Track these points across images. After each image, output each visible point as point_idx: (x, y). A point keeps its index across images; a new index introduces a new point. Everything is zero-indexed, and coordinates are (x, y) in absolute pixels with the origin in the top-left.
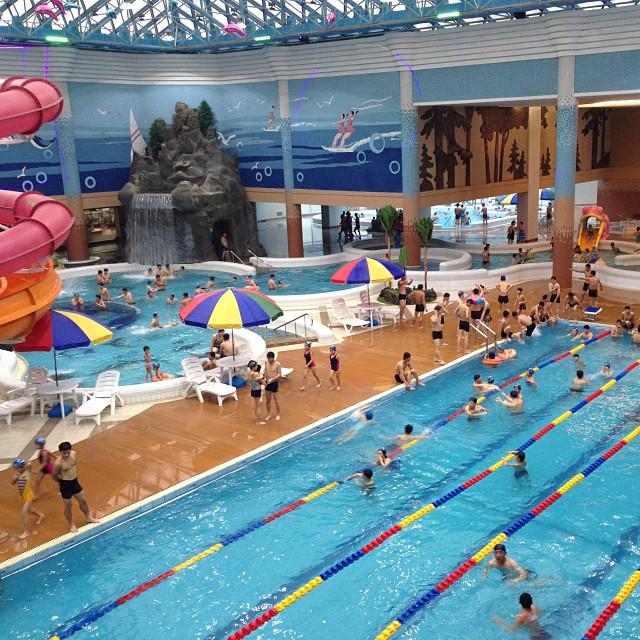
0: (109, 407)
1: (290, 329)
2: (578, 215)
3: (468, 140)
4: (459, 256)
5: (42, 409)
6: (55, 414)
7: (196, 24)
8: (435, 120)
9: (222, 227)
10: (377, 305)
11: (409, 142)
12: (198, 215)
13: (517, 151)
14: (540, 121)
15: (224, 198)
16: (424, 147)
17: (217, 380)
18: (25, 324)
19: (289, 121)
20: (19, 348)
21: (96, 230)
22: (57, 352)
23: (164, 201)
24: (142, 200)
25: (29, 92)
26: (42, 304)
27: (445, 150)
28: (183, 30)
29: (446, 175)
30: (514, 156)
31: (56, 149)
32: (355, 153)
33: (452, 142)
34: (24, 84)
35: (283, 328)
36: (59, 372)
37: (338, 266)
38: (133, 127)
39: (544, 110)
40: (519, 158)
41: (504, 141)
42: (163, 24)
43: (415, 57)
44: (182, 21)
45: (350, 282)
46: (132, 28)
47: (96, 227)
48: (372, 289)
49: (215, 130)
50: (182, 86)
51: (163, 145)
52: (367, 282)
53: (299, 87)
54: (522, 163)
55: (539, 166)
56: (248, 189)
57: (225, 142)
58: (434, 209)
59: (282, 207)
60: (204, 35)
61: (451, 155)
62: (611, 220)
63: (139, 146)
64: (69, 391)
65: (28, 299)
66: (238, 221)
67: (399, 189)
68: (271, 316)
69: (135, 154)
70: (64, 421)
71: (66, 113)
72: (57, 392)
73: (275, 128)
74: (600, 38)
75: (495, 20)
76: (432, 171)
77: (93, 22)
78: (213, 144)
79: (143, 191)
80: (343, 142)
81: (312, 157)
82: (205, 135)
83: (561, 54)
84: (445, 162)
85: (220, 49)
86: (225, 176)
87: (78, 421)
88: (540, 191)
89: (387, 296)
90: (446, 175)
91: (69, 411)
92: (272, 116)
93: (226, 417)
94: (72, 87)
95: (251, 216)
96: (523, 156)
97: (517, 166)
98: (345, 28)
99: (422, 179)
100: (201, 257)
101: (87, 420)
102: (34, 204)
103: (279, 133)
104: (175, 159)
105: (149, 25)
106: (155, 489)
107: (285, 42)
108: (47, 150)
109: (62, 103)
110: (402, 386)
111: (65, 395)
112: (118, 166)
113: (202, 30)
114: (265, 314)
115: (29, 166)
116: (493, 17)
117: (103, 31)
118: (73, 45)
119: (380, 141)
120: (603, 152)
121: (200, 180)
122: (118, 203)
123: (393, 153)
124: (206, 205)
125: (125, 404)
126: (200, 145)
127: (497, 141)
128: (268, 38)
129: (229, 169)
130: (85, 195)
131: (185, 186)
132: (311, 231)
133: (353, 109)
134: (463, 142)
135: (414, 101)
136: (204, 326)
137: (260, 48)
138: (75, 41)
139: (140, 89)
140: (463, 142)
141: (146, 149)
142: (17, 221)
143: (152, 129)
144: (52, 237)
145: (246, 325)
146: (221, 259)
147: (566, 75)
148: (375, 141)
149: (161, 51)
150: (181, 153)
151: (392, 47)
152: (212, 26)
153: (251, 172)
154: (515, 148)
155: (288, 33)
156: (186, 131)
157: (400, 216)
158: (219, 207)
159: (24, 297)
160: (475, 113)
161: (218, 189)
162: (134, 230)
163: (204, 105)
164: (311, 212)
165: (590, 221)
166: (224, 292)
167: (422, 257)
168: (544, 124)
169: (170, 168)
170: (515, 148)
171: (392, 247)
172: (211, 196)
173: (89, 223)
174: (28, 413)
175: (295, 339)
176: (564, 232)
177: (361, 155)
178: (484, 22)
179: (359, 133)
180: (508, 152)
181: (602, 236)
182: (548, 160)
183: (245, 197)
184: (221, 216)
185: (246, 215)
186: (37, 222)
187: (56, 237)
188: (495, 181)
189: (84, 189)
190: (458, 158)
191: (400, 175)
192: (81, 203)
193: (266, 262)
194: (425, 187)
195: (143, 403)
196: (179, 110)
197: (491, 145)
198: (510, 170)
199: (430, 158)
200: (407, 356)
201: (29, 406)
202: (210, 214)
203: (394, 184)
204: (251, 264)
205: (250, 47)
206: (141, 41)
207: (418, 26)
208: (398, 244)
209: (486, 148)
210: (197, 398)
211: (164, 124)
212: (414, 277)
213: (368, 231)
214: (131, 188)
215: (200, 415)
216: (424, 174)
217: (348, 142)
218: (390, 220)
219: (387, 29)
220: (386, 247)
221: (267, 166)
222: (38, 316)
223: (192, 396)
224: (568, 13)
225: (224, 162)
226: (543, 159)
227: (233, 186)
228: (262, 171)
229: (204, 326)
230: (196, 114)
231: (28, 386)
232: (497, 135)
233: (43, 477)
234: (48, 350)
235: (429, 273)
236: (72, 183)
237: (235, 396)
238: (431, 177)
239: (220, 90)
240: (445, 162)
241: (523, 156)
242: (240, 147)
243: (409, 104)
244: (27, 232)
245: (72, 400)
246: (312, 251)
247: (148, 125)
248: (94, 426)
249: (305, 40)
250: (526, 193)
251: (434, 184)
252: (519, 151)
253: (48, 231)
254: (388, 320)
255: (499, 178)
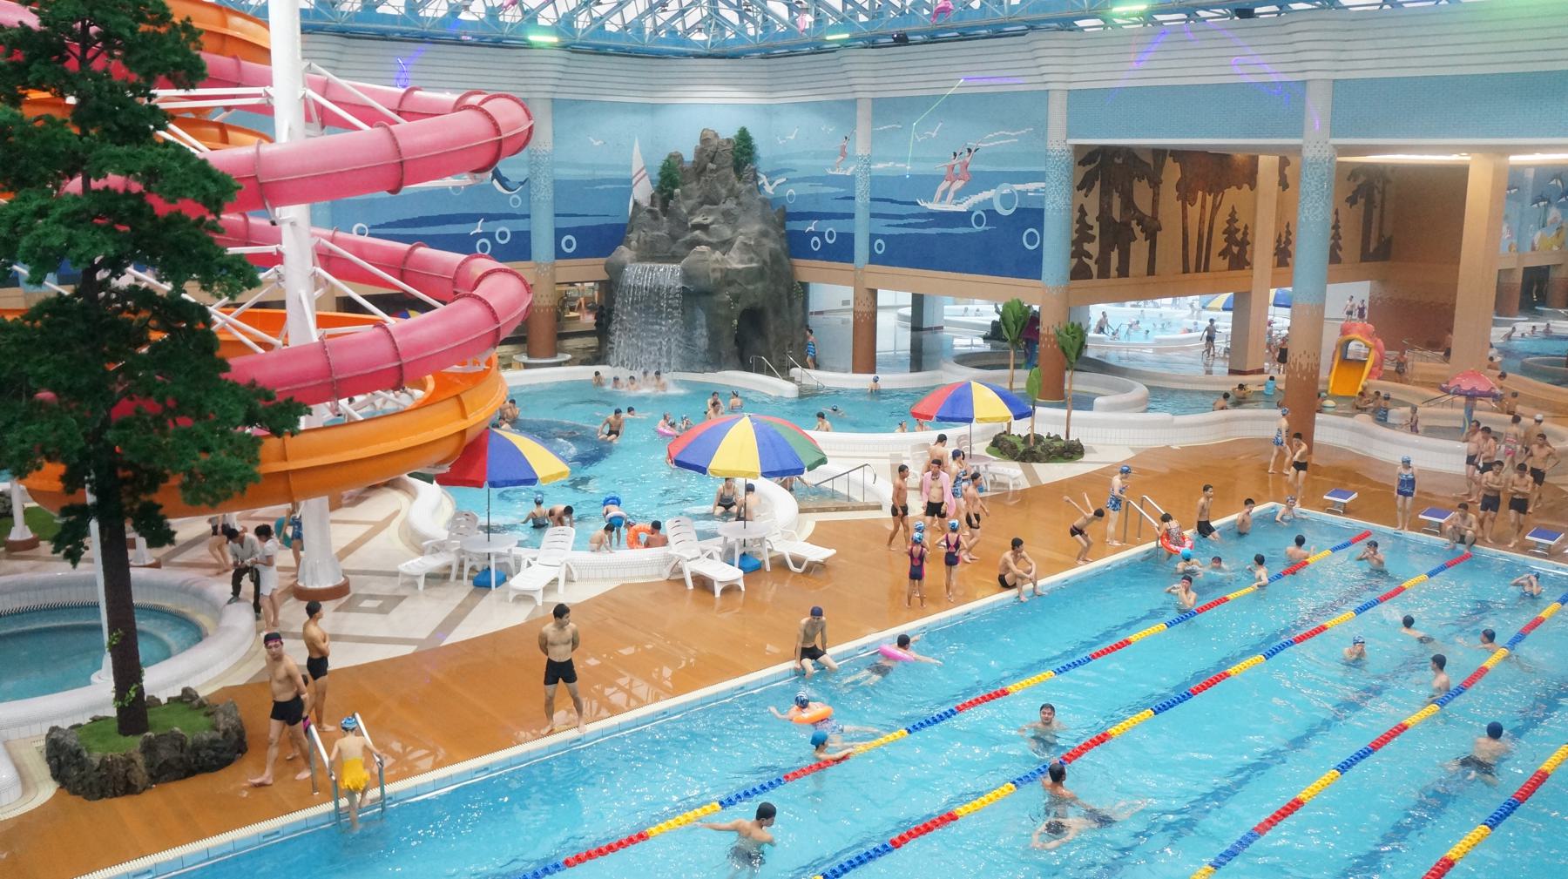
0: (556, 580)
1: (840, 487)
2: (1331, 337)
3: (1155, 202)
4: (1126, 390)
5: (466, 569)
6: (482, 583)
7: (742, 16)
8: (1104, 170)
9: (753, 319)
10: (985, 458)
11: (1057, 202)
12: (717, 298)
13: (1236, 225)
14: (1277, 178)
15: (760, 274)
16: (1082, 210)
17: (717, 557)
18: (450, 448)
19: (869, 161)
20: (444, 481)
21: (572, 314)
22: (495, 491)
23: (668, 275)
24: (640, 274)
25: (487, 114)
26: (477, 418)
27: (1116, 214)
28: (721, 25)
29: (1115, 255)
30: (1230, 233)
31: (527, 196)
32: (970, 213)
33: (1128, 204)
34: (483, 102)
35: (828, 485)
36: (494, 521)
37: (923, 391)
38: (637, 163)
39: (1284, 163)
40: (1239, 236)
41: (1215, 208)
42: (694, 17)
43: (1074, 70)
44: (722, 12)
45: (941, 419)
46: (648, 23)
47: (572, 309)
48: (975, 436)
49: (755, 171)
50: (711, 107)
51: (677, 191)
52: (969, 420)
53: (885, 109)
54: (1244, 244)
55: (1272, 251)
56: (798, 262)
57: (769, 189)
58: (1096, 311)
59: (848, 292)
60: (751, 32)
61: (1127, 225)
62: (1388, 348)
63: (643, 192)
64: (504, 550)
65: (457, 410)
66: (777, 312)
67: (1037, 275)
68: (807, 463)
69: (636, 203)
70: (495, 593)
71: (543, 140)
72: (488, 550)
73: (846, 169)
74: (1376, 54)
75: (1204, 20)
76: (1093, 248)
77: (595, 15)
78: (750, 191)
79: (641, 259)
80: (951, 195)
81: (901, 217)
82: (740, 178)
83: (1309, 76)
84: (1116, 235)
85: (775, 54)
86: (765, 241)
87: (512, 595)
88: (1273, 292)
89: (1003, 446)
90: (1115, 255)
91: (502, 580)
92: (843, 154)
93: (725, 616)
94: (557, 105)
95: (798, 305)
96: (1245, 234)
97: (1235, 249)
98: (966, 23)
99: (1075, 261)
100: (716, 362)
101: (524, 597)
102: (480, 273)
103: (853, 177)
104: (691, 212)
105: (673, 18)
106: (614, 710)
107: (873, 43)
108: (514, 195)
109: (531, 128)
110: (1009, 594)
111: (498, 556)
112: (609, 221)
113: (750, 25)
114: (797, 460)
115: (489, 218)
116: (1202, 14)
117: (608, 27)
118: (564, 47)
119: (1012, 195)
120: (1381, 236)
121: (725, 245)
122: (604, 276)
123: (1031, 216)
124: (730, 283)
125: (580, 579)
126: (733, 194)
127: (1203, 207)
128: (846, 36)
129: (773, 232)
130: (559, 262)
131: (703, 253)
132: (892, 334)
133: (970, 144)
134: (1145, 208)
135: (1069, 136)
136: (703, 470)
137: (833, 51)
138: (568, 41)
139: (653, 109)
140: (1145, 208)
141: (653, 197)
142: (456, 296)
143: (663, 168)
144: (496, 320)
145: (767, 474)
146: (745, 366)
147: (1317, 110)
148: (1003, 197)
149: (687, 55)
150: (702, 204)
151: (852, 81)
152: (765, 20)
153: (799, 238)
154: (1232, 219)
155: (877, 29)
156: (712, 171)
157: (1035, 319)
158: (751, 287)
159: (452, 405)
160: (1169, 160)
161: (751, 260)
162: (624, 312)
163: (743, 132)
164: (894, 306)
165: (1352, 346)
166: (738, 419)
167: (1066, 387)
168: (1284, 184)
169: (683, 225)
170: (1232, 219)
171: (1017, 367)
172: (738, 271)
173: (564, 303)
174: (446, 577)
175: (845, 503)
176: (1304, 362)
177: (979, 218)
178: (1187, 21)
179: (977, 182)
180: (1221, 223)
181: (1371, 372)
182: (1288, 242)
183: (791, 275)
184: (752, 300)
185: (791, 303)
186: (480, 299)
187: (502, 322)
188: (1197, 270)
189: (560, 254)
190: (1137, 229)
191: (1039, 253)
192: (553, 276)
193: (813, 377)
194: (1079, 272)
195: (604, 579)
196: (705, 140)
197: (1194, 211)
198: (1223, 254)
199: (1091, 228)
200: (1017, 544)
201: (450, 567)
202: (736, 298)
203: (1030, 266)
204: (792, 380)
205: (819, 49)
206: (662, 41)
207: (1080, 23)
208: (1029, 360)
209: (1185, 217)
210: (683, 581)
211: (681, 160)
212: (1048, 421)
213: (985, 338)
214: (624, 253)
215: (686, 608)
216: (1078, 252)
217: (959, 195)
218: (1015, 323)
219: (1032, 27)
220: (1006, 367)
221: (830, 227)
222: (470, 437)
223: (677, 580)
224: (1325, 14)
225: (764, 220)
226: (1279, 241)
227: (775, 258)
228: (821, 235)
229: (703, 470)
230: (730, 147)
231: (451, 538)
232: (1204, 200)
233: (949, 573)
234: (480, 485)
235: (1075, 413)
236: (542, 245)
237: (741, 584)
238: (1090, 257)
239: (768, 111)
240: (1116, 235)
241: (1245, 234)
242: (791, 196)
243: (1060, 141)
244: (465, 313)
245: (506, 564)
246: (893, 364)
247: (659, 163)
248: (532, 607)
249: (902, 40)
250: (1249, 293)
251: (1094, 269)
252: (1240, 225)
253: (493, 313)
254: (1000, 484)
255: (1203, 266)
